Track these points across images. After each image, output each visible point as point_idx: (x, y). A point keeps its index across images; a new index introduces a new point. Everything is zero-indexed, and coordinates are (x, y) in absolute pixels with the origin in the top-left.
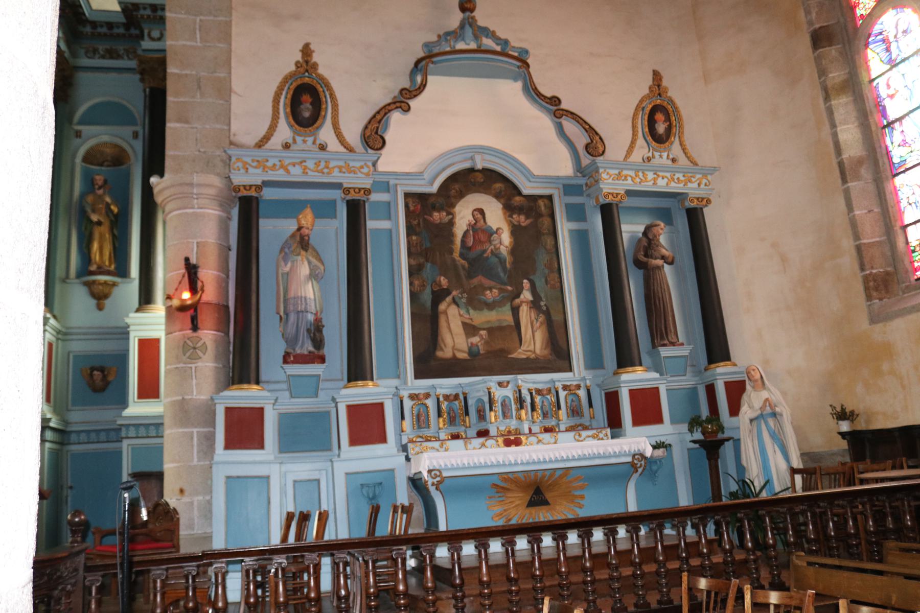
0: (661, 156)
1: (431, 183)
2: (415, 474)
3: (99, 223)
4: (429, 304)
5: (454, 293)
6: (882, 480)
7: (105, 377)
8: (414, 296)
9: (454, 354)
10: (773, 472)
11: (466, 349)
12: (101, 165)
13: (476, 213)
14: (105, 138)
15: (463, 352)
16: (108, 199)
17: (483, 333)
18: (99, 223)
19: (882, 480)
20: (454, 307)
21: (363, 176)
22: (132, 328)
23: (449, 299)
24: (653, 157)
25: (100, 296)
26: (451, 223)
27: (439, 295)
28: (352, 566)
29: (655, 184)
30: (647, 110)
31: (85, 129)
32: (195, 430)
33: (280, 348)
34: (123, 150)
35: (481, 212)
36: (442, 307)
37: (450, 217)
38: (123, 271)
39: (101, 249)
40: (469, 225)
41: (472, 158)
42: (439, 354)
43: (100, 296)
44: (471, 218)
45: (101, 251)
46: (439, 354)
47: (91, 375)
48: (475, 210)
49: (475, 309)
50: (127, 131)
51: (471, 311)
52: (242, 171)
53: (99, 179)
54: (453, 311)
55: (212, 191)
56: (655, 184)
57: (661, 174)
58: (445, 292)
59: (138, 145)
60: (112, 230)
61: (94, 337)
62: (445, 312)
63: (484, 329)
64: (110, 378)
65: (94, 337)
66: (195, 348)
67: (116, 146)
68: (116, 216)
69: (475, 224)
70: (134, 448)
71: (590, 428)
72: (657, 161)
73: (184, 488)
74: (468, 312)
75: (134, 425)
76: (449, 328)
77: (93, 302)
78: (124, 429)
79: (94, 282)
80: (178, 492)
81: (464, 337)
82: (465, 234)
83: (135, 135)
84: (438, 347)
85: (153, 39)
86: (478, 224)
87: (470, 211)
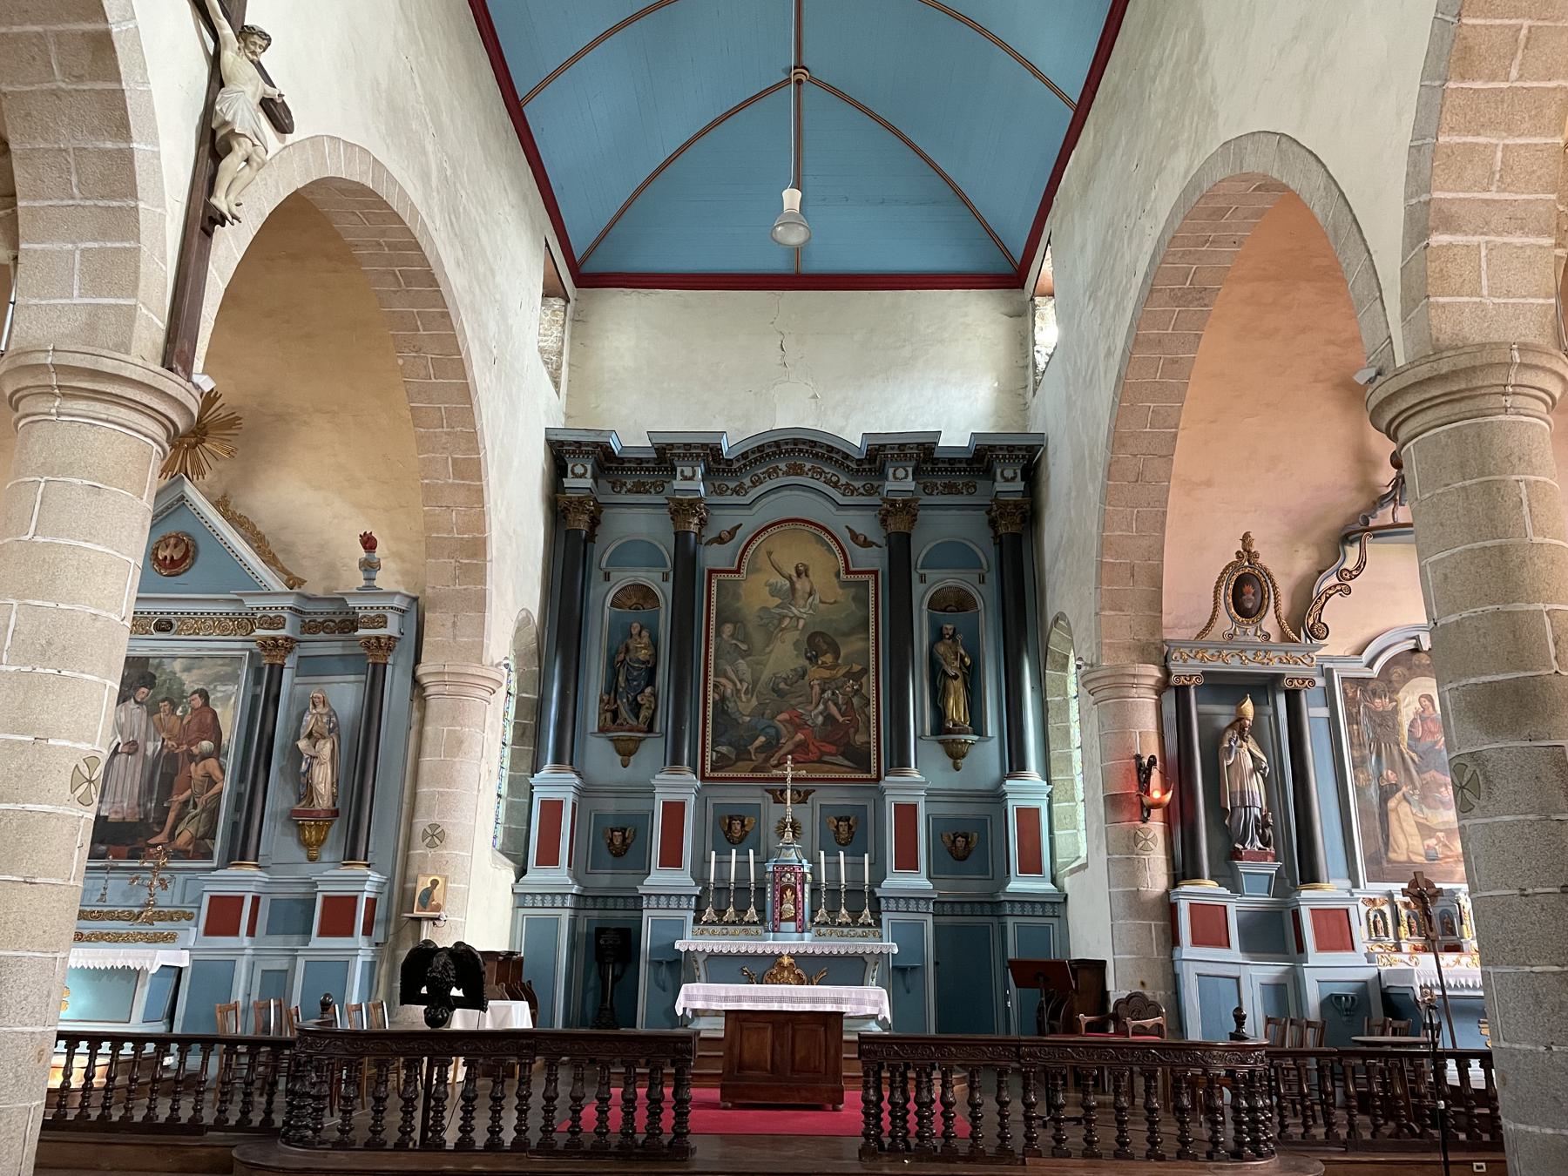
1: (1370, 665)
2: (1389, 987)
3: (956, 677)
4: (1375, 801)
5: (1404, 789)
7: (967, 843)
8: (1360, 791)
9: (1409, 857)
10: (101, 385)
11: (1422, 852)
13: (1423, 699)
14: (951, 583)
15: (1421, 855)
16: (962, 652)
17: (1440, 834)
20: (1405, 804)
21: (1306, 667)
22: (1009, 796)
23: (1400, 794)
25: (956, 754)
26: (1396, 711)
27: (1386, 794)
28: (722, 1104)
31: (932, 575)
32: (1153, 923)
34: (969, 595)
36: (1392, 804)
37: (1394, 704)
38: (979, 728)
39: (957, 704)
42: (1392, 855)
43: (956, 754)
44: (1418, 706)
45: (956, 709)
46: (1392, 855)
47: (954, 842)
48: (1421, 696)
49: (1429, 807)
51: (1425, 810)
52: (1181, 662)
54: (1404, 807)
55: (1152, 682)
58: (1395, 788)
59: (669, 586)
61: (946, 799)
62: (1396, 810)
63: (1441, 831)
64: (972, 846)
65: (946, 799)
66: (1146, 840)
68: (968, 668)
70: (1019, 926)
73: (1146, 981)
74: (1421, 810)
75: (1019, 902)
76: (1402, 828)
77: (951, 761)
78: (1008, 905)
80: (1139, 984)
81: (1419, 838)
82: (1412, 725)
84: (1390, 848)
85: (1007, 480)
86: (1426, 712)
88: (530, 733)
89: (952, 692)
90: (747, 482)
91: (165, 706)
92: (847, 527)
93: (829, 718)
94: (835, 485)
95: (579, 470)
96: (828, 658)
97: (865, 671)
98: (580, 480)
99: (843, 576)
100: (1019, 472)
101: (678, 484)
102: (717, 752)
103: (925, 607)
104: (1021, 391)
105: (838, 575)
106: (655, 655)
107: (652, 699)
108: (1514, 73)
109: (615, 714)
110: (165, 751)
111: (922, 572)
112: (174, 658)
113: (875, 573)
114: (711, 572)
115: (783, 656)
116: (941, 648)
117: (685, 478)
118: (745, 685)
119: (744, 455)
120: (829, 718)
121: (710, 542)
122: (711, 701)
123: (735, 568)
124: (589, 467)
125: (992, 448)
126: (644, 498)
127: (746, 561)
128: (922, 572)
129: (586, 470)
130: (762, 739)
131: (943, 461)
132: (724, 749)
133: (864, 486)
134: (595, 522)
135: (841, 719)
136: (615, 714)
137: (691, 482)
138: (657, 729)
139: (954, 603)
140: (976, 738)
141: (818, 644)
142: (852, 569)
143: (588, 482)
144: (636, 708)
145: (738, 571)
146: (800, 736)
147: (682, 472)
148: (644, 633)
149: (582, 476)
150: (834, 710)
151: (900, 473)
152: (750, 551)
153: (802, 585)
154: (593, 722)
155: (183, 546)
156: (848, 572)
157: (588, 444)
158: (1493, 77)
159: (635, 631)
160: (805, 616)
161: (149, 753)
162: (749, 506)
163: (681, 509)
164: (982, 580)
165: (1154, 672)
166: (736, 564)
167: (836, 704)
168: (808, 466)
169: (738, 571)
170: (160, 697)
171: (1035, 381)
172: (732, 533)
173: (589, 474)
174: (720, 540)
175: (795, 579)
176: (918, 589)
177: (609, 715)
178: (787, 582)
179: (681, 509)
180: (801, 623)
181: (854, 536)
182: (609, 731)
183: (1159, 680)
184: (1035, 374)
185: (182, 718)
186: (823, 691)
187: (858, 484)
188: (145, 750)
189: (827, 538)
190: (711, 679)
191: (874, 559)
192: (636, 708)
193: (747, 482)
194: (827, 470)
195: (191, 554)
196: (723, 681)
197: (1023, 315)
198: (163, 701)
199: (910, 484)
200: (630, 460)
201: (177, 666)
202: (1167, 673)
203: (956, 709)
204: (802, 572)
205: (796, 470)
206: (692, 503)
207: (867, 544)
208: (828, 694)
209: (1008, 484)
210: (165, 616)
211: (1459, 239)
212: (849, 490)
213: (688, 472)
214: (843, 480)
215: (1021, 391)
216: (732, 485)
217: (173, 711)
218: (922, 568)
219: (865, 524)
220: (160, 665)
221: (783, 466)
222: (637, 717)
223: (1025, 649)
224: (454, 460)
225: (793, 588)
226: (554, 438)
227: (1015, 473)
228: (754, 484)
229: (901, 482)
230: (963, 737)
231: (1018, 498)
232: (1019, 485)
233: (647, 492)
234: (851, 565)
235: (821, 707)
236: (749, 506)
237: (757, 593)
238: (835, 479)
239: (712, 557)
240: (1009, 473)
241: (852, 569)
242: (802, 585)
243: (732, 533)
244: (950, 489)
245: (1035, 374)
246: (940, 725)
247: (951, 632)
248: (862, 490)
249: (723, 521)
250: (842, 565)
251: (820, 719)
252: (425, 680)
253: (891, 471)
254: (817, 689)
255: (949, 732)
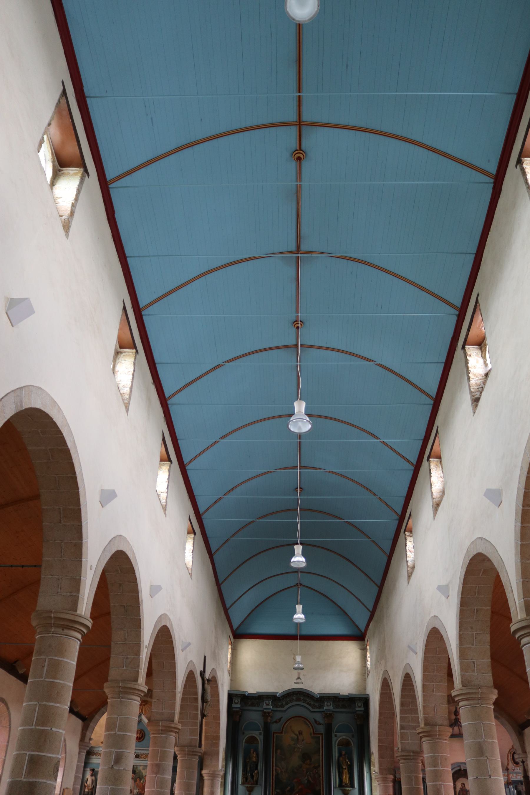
0: (517, 769)
3: (345, 769)
6: (322, 742)
12: (342, 746)
14: (344, 737)
16: (347, 760)
18: (345, 769)
19: (322, 742)
24: (515, 769)
29: (516, 778)
30: (512, 753)
33: (148, 767)
35: (464, 784)
38: (352, 786)
40: (460, 788)
41: (460, 766)
44: (461, 786)
45: (345, 778)
50: (257, 732)
53: (343, 752)
55: (391, 779)
56: (516, 778)
57: (518, 774)
59: (262, 737)
60: (348, 770)
67: (347, 740)
68: (349, 765)
69: (462, 788)
71: (410, 575)
72: (516, 771)
79: (345, 789)
83: (260, 734)
87: (460, 784)
88: (223, 784)
89: (344, 773)
90: (284, 703)
91: (138, 779)
92: (314, 719)
93: (309, 781)
94: (310, 705)
95: (236, 701)
96: (308, 761)
97: (319, 766)
98: (237, 705)
99: (312, 735)
100: (362, 704)
101: (265, 706)
102: (276, 792)
103: (336, 745)
104: (364, 674)
105: (311, 734)
106: (258, 760)
107: (257, 774)
108: (411, 706)
109: (247, 779)
110: (139, 793)
111: (335, 733)
112: (140, 766)
113: (322, 734)
114: (274, 733)
115: (295, 761)
116: (341, 759)
117: (267, 705)
118: (284, 770)
119: (283, 696)
120: (309, 781)
121: (273, 723)
122: (274, 775)
123: (281, 731)
124: (239, 700)
125: (354, 698)
126: (254, 708)
127: (284, 730)
128: (335, 733)
129: (238, 702)
130: (289, 788)
131: (341, 698)
132: (278, 791)
133: (318, 705)
134: (240, 716)
135: (312, 782)
136: (247, 779)
137: (268, 706)
138: (259, 784)
139: (345, 744)
140: (351, 788)
141: (305, 757)
142: (315, 733)
143: (239, 706)
144: (252, 777)
145: (282, 733)
146: (300, 787)
147: (266, 703)
148: (255, 753)
149: (237, 703)
150: (310, 779)
151: (329, 704)
152: (285, 726)
153: (301, 738)
154: (240, 781)
155: (141, 733)
156: (314, 734)
157: (239, 694)
158: (408, 707)
159: (252, 752)
160: (301, 748)
161: (135, 793)
162: (285, 711)
163: (265, 715)
164: (353, 736)
165: (392, 777)
166: (281, 730)
167: (311, 777)
168: (302, 698)
169: (282, 733)
170: (137, 777)
171: (367, 673)
172: (280, 719)
173: (239, 703)
174: (276, 722)
175: (298, 735)
176: (334, 739)
177: (245, 779)
178: (296, 736)
179: (265, 715)
180: (300, 750)
181: (316, 721)
182: (245, 784)
183: (393, 779)
184: (368, 671)
185: (143, 783)
186: (307, 772)
187: (317, 704)
188: (134, 792)
189: (308, 722)
190: (274, 767)
191: (321, 729)
192: (252, 777)
193: (284, 703)
194: (307, 700)
195: (144, 736)
196: (278, 768)
197: (364, 650)
198: (138, 778)
199: (331, 708)
200: (250, 697)
201: (141, 768)
202: (395, 777)
203: (345, 778)
204: (300, 733)
205: (298, 700)
206: (269, 713)
207: (319, 724)
208: (308, 773)
209: (360, 709)
210: (138, 754)
211: (405, 731)
212: (314, 707)
213: (267, 702)
214: (312, 703)
215: (364, 674)
216: (280, 704)
217: (140, 781)
218: (335, 732)
219: (319, 717)
220: (137, 768)
221: (294, 698)
222: (253, 780)
223: (366, 758)
224: (213, 716)
225: (298, 739)
226: (230, 693)
227: (361, 705)
228: (287, 704)
229: (329, 707)
230: (347, 788)
231: (362, 713)
232: (362, 709)
233: (255, 706)
234: (315, 732)
235: (306, 777)
236: (285, 711)
237: (287, 739)
238: (310, 703)
239: (274, 727)
240: (360, 705)
241: (315, 733)
242: (301, 738)
243: (280, 719)
244: (344, 707)
245: (368, 671)
246: (341, 785)
247: (344, 754)
248: (318, 707)
249: (278, 716)
250: (312, 731)
251: (306, 781)
252: (204, 775)
253: (326, 703)
254: (305, 771)
255: (344, 786)
